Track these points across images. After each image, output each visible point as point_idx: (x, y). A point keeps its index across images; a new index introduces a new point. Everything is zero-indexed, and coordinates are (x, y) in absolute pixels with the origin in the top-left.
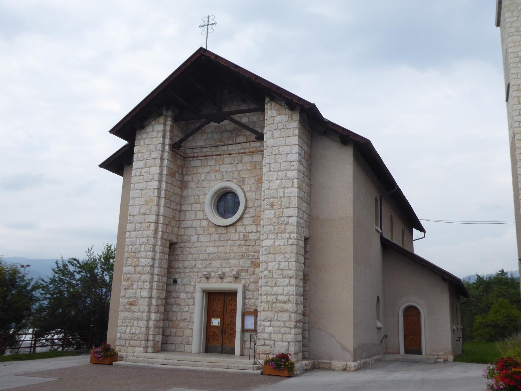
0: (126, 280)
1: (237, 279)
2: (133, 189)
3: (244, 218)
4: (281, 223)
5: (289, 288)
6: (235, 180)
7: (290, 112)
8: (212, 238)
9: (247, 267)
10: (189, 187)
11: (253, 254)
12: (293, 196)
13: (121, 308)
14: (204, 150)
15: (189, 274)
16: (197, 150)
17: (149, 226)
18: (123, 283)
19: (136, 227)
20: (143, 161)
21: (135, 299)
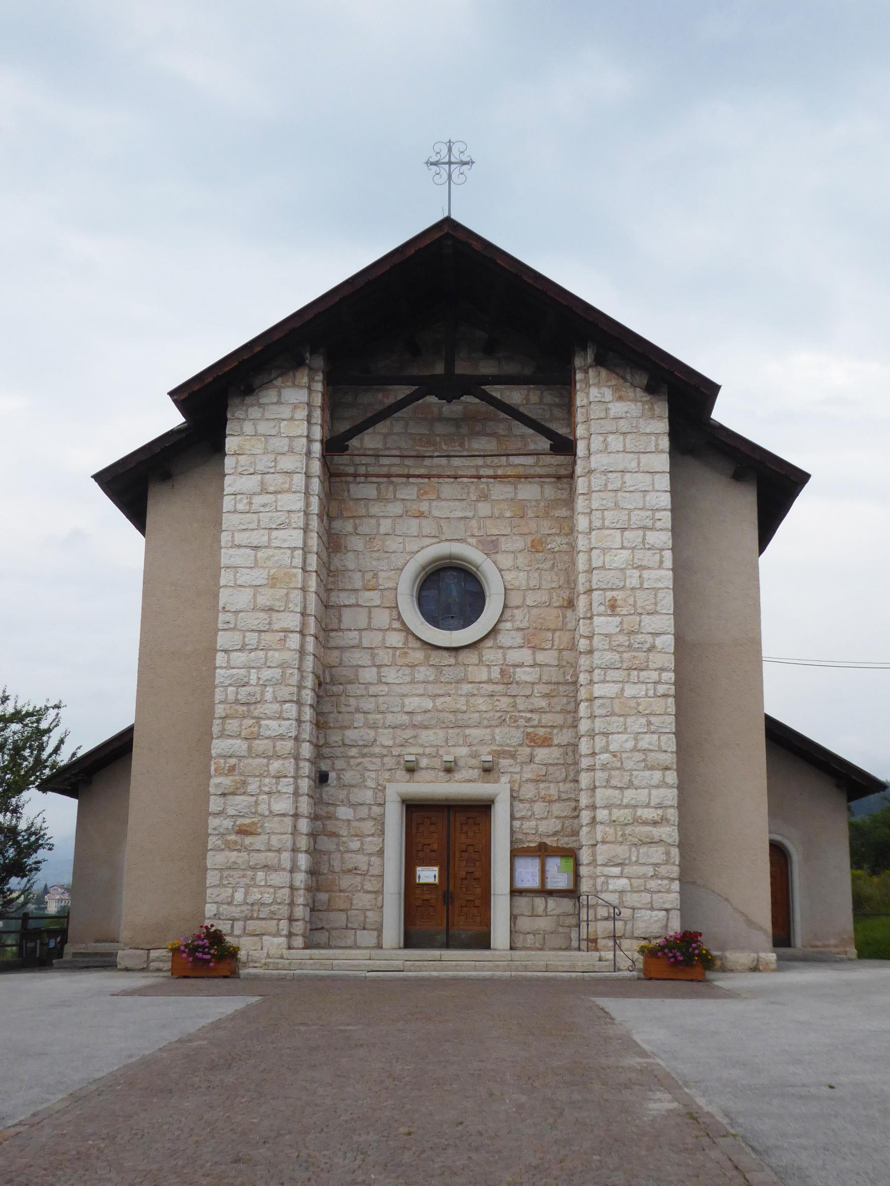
0: (226, 772)
1: (488, 773)
2: (230, 544)
3: (501, 632)
4: (636, 646)
5: (663, 791)
6: (473, 541)
7: (647, 398)
8: (416, 676)
9: (514, 747)
10: (346, 547)
11: (529, 715)
12: (663, 589)
13: (212, 841)
14: (385, 461)
15: (360, 760)
16: (365, 460)
17: (284, 640)
18: (214, 781)
19: (247, 639)
20: (253, 476)
21: (256, 820)
